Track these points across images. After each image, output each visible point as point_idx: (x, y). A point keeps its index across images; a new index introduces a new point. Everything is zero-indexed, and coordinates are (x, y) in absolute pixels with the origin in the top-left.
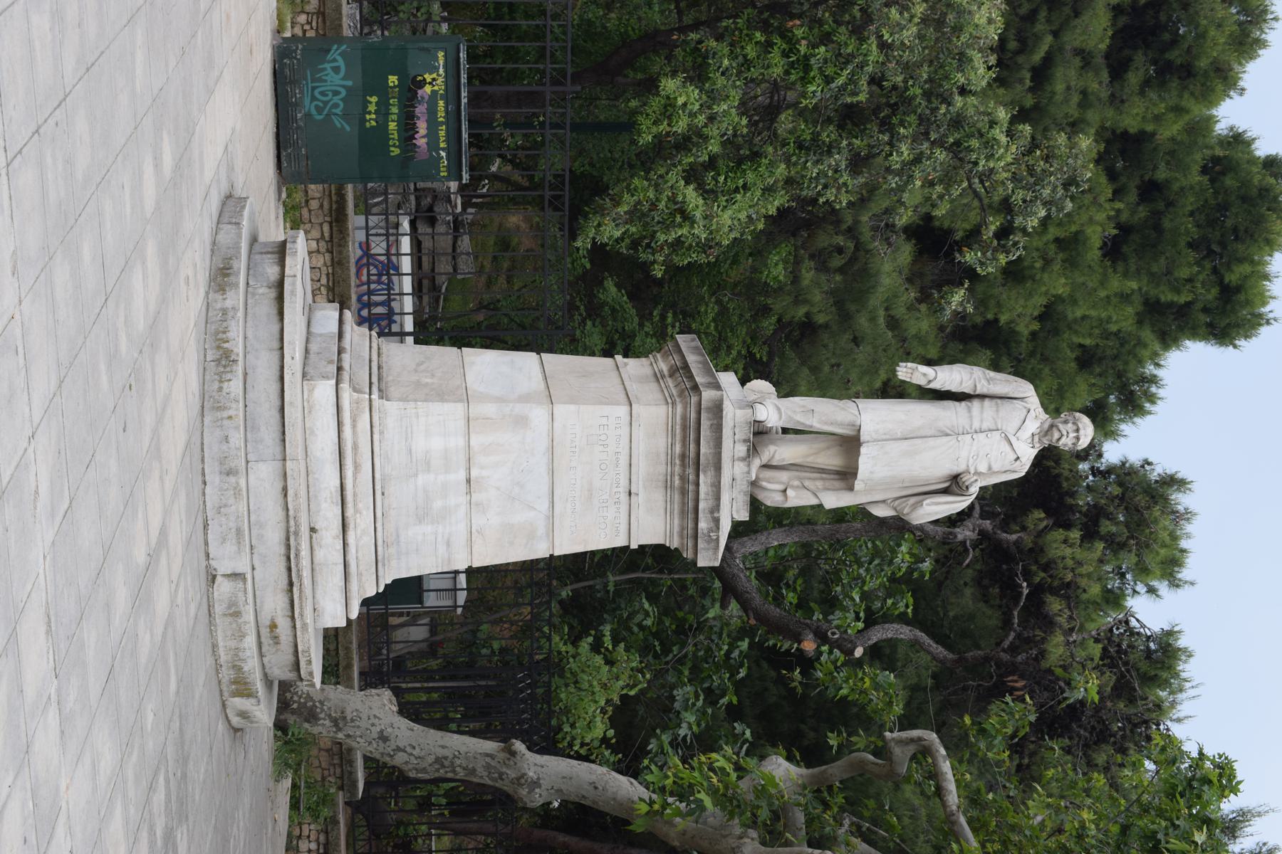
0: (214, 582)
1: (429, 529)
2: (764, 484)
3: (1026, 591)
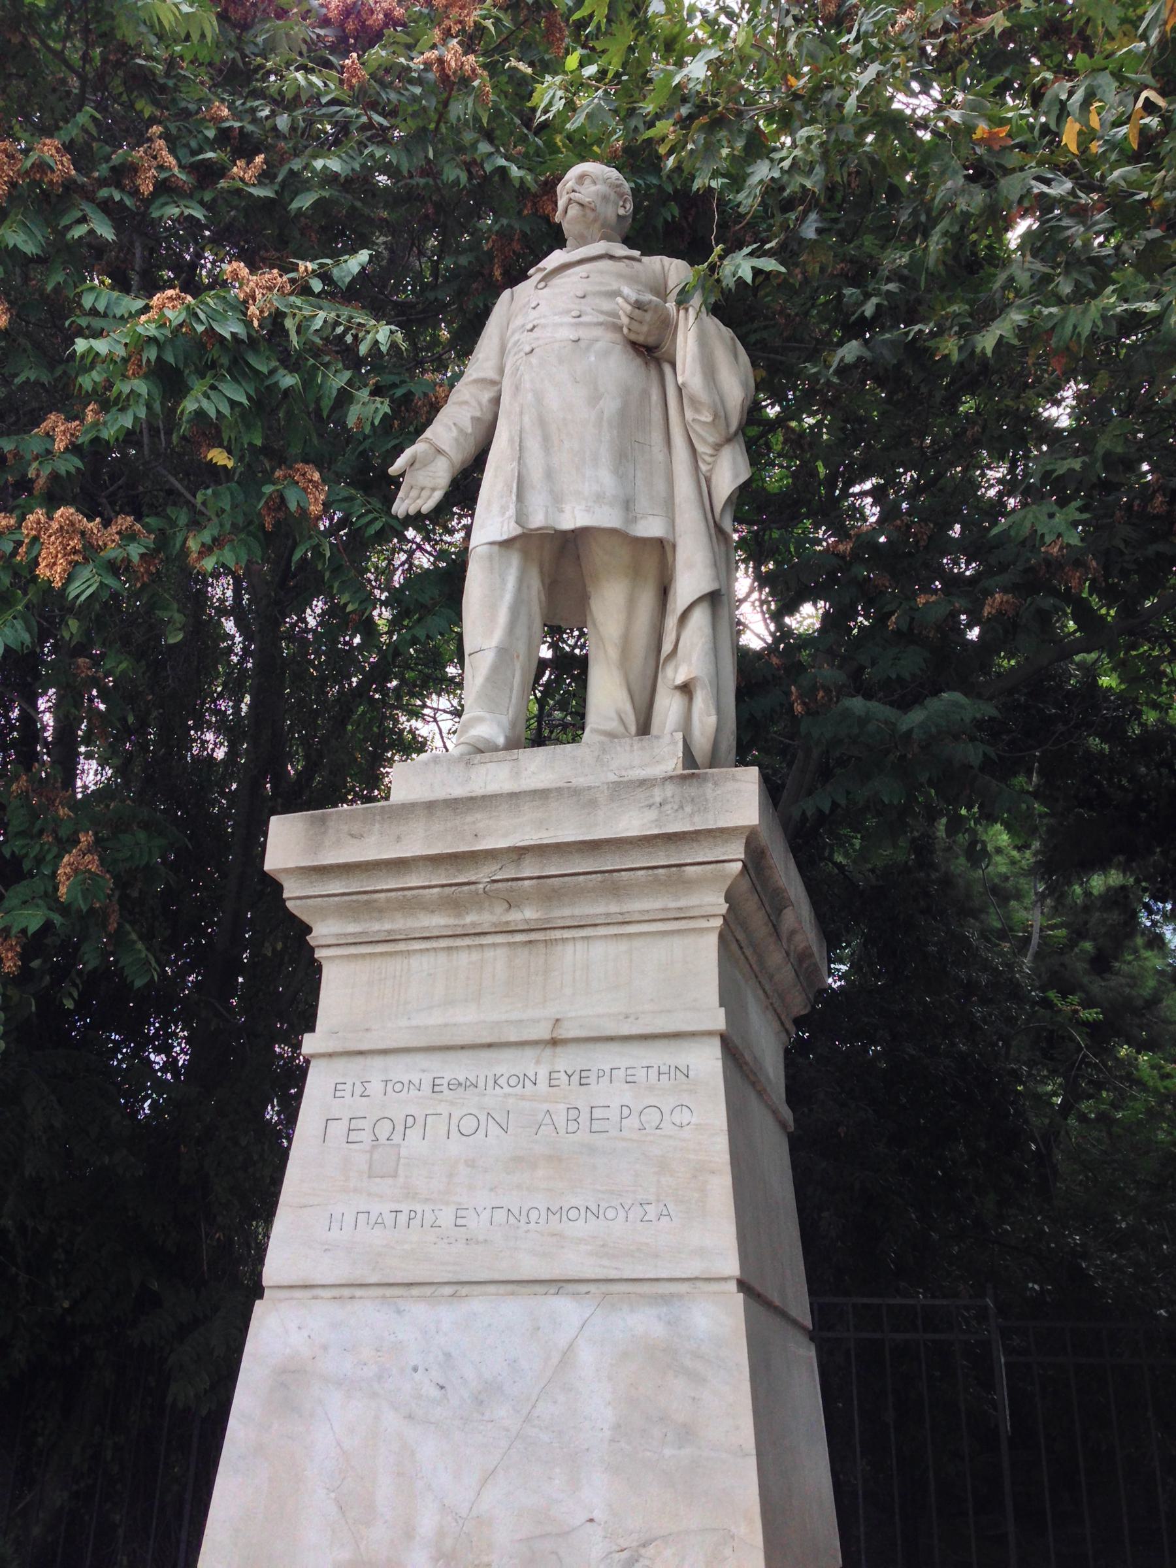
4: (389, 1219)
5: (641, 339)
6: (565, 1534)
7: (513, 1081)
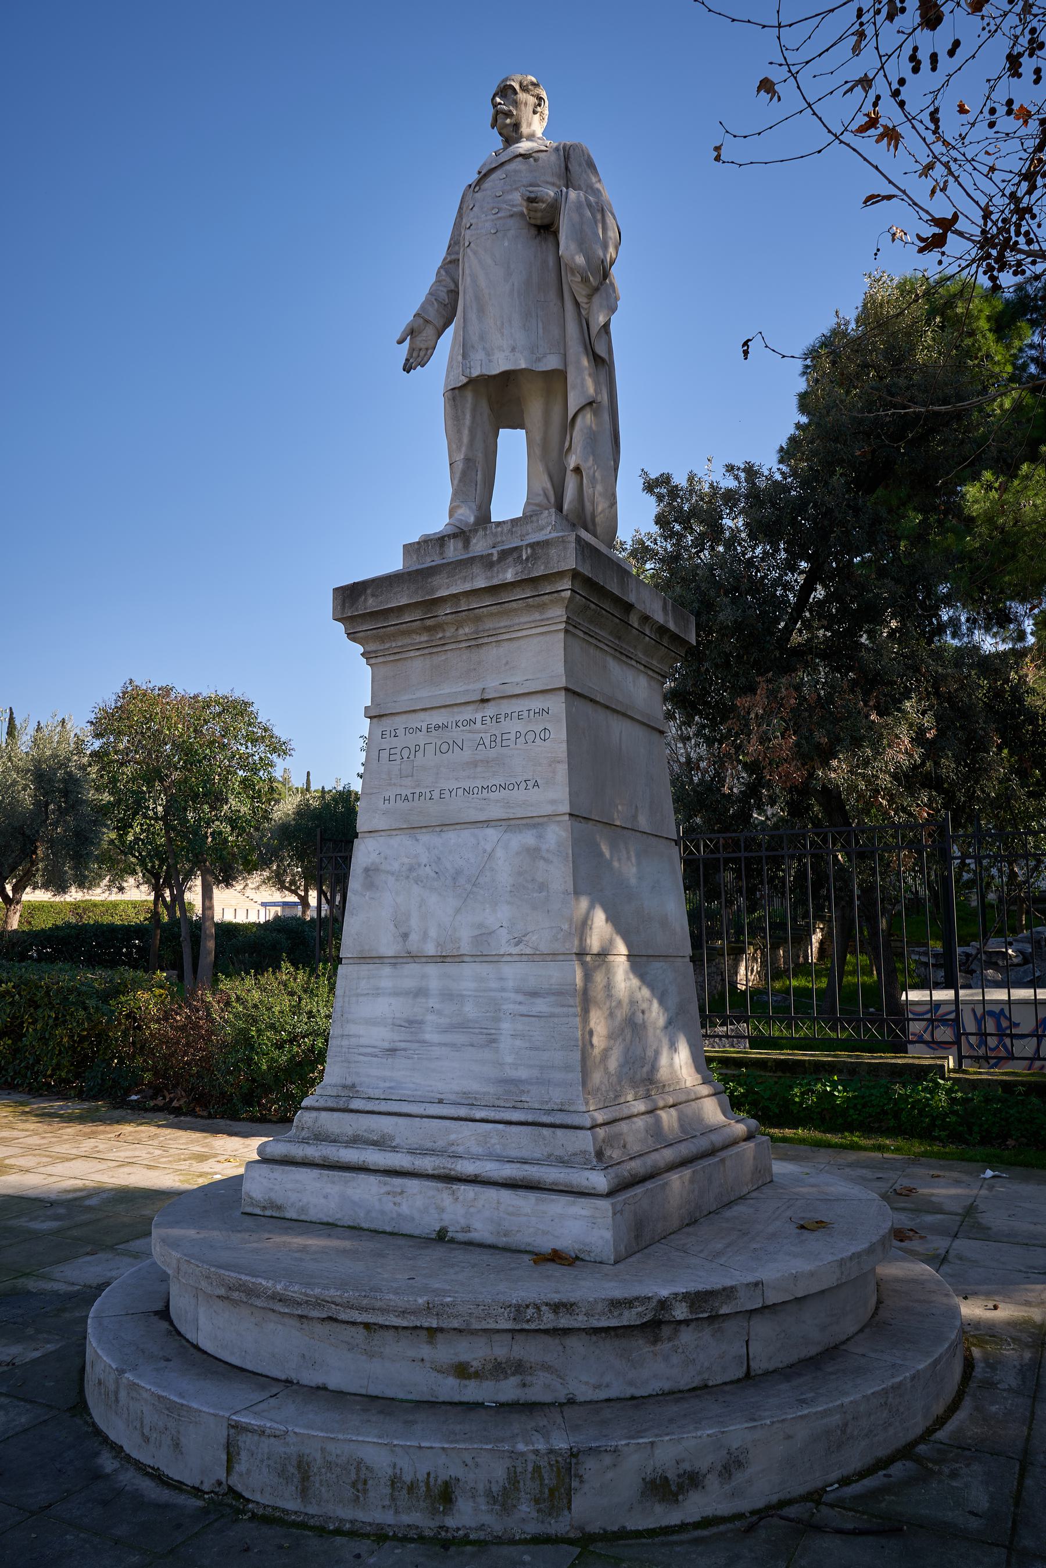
1: (506, 1026)
4: (410, 797)
5: (539, 222)
6: (494, 932)
7: (465, 723)
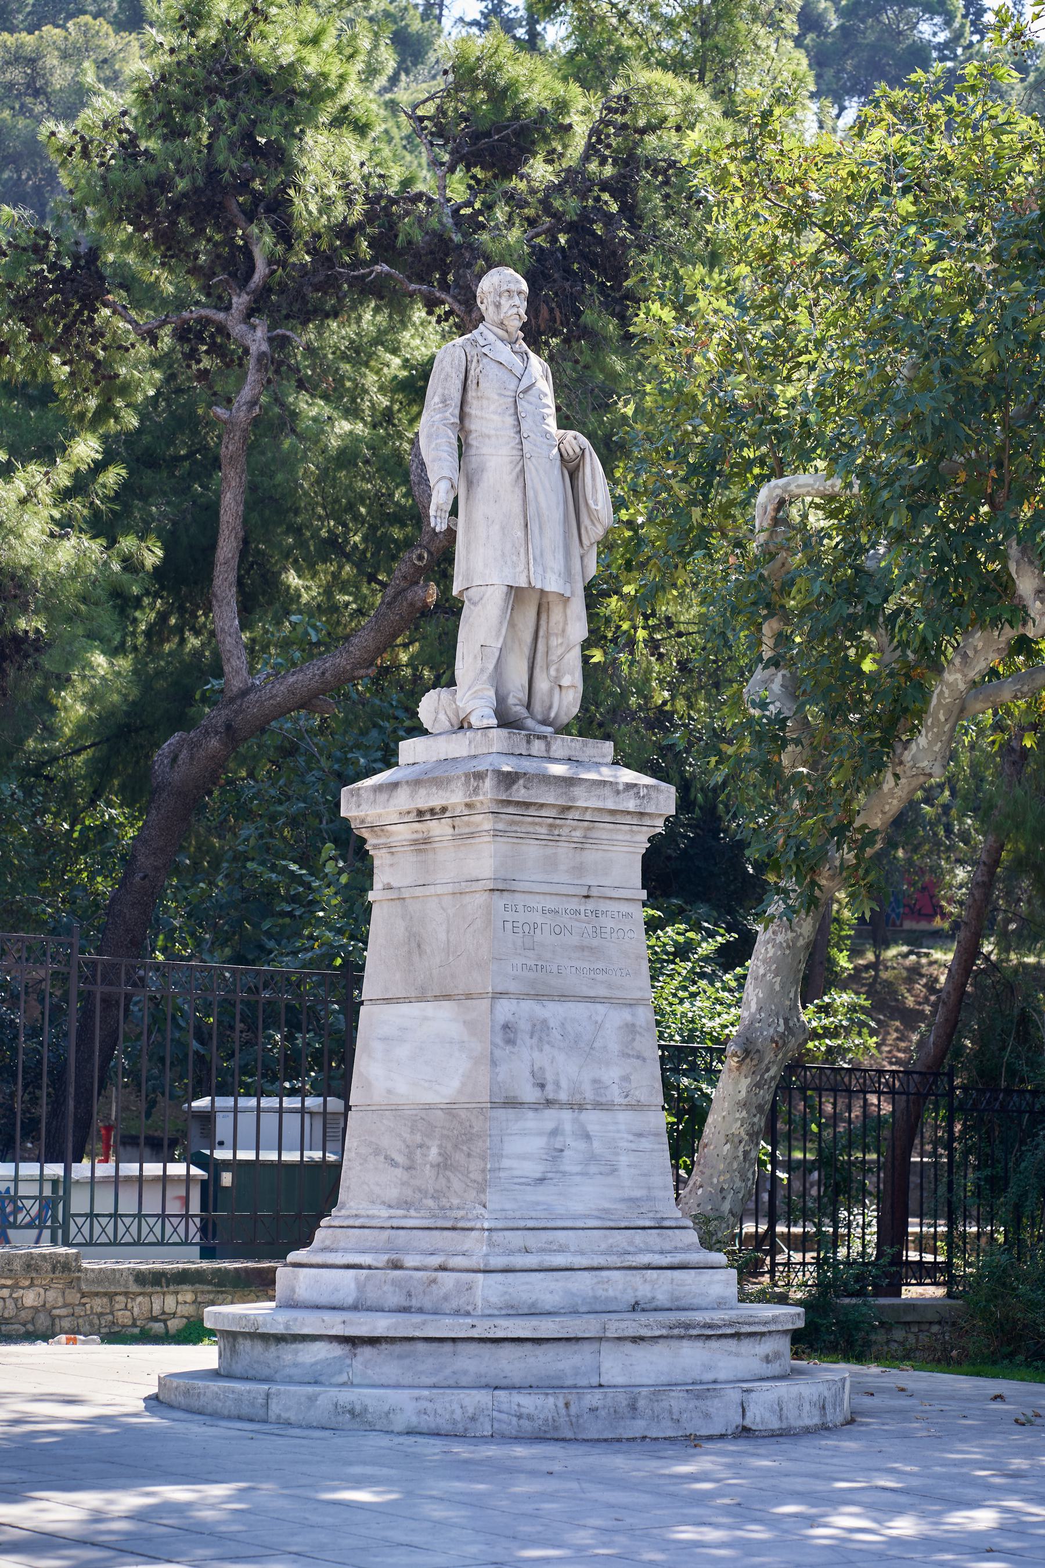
0: (750, 1430)
2: (552, 715)
3: (386, 268)
